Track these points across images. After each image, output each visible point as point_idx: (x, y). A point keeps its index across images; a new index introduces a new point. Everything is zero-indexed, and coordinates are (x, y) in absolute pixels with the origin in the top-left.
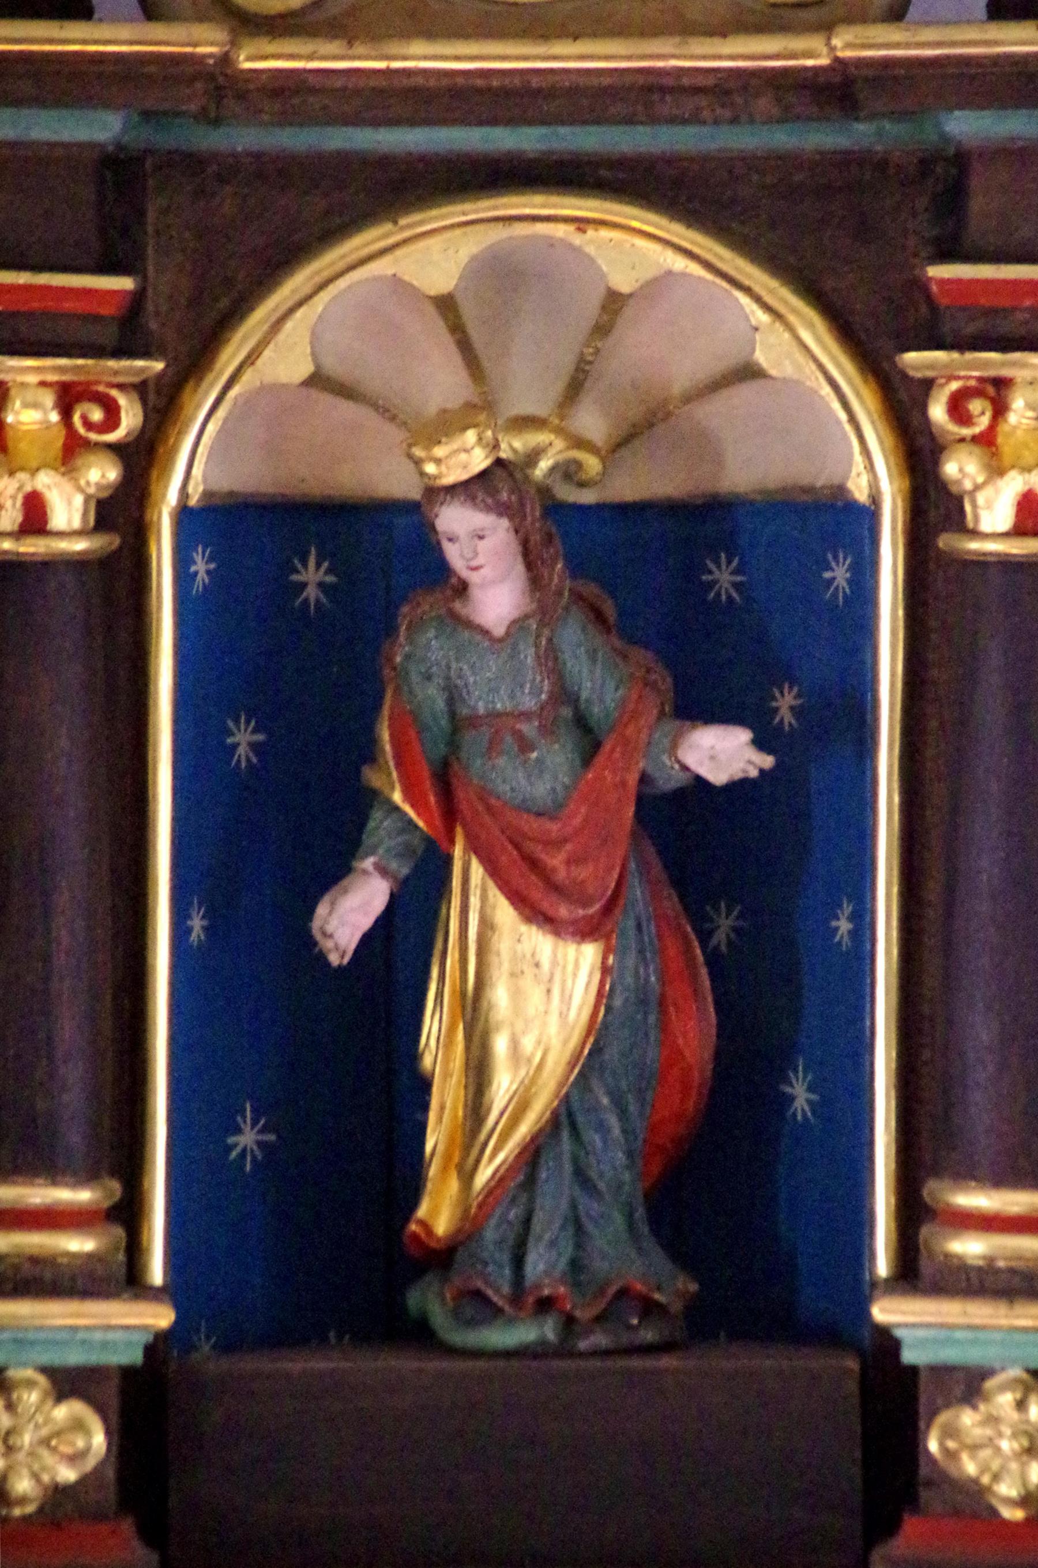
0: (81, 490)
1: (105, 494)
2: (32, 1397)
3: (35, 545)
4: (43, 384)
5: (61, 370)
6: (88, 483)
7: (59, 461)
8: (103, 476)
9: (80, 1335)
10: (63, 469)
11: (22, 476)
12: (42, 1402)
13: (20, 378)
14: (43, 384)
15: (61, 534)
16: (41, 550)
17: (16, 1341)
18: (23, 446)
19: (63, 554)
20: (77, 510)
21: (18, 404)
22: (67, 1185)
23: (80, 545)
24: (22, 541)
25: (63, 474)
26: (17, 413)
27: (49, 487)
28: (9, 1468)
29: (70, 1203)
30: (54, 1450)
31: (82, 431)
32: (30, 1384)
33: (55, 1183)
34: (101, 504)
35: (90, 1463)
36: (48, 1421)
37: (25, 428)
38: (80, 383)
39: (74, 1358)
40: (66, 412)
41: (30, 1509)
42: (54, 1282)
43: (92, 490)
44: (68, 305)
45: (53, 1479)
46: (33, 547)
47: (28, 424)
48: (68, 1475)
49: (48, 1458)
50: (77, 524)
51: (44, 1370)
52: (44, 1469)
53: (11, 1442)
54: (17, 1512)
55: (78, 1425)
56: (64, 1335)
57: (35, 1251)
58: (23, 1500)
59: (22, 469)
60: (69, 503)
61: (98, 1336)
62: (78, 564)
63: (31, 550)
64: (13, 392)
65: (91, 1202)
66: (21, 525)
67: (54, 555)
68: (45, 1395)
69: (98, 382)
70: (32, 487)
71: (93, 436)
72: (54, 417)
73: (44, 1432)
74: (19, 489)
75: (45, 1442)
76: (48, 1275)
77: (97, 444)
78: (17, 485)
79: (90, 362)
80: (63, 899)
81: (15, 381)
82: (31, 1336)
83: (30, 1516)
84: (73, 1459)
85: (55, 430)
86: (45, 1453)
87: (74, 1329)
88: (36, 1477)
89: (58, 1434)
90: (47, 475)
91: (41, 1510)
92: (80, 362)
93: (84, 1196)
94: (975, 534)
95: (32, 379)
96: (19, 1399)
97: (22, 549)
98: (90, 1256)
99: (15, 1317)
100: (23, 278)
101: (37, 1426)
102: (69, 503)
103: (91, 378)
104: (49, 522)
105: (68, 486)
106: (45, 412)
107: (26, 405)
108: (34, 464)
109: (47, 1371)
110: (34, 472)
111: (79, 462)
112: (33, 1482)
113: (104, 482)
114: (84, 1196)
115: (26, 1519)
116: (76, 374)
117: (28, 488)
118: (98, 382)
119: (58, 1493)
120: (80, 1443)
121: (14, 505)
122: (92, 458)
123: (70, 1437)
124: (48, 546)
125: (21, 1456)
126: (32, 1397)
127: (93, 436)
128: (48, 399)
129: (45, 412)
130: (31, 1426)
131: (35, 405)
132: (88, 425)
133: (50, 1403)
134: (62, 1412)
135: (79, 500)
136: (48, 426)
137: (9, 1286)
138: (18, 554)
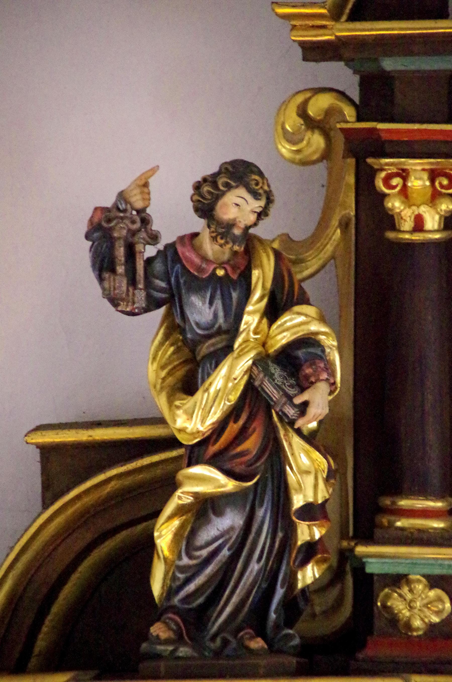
0: (438, 213)
1: (447, 215)
2: (420, 587)
3: (419, 236)
4: (424, 170)
5: (431, 164)
6: (441, 210)
7: (429, 201)
8: (448, 207)
9: (440, 562)
10: (430, 205)
11: (414, 208)
12: (424, 589)
13: (413, 168)
14: (424, 170)
15: (404, 232)
16: (421, 238)
17: (412, 563)
18: (415, 195)
19: (431, 239)
20: (436, 221)
21: (413, 178)
22: (432, 500)
23: (437, 236)
24: (413, 235)
25: (431, 207)
26: (412, 182)
27: (425, 212)
28: (412, 616)
29: (433, 507)
30: (429, 608)
31: (439, 189)
32: (419, 581)
33: (427, 499)
34: (446, 219)
35: (445, 615)
36: (427, 597)
37: (415, 188)
38: (439, 169)
39: (437, 571)
40: (432, 180)
41: (420, 633)
42: (428, 540)
43: (443, 213)
44: (435, 138)
45: (430, 621)
46: (418, 237)
47: (417, 186)
48: (435, 619)
49: (428, 613)
50: (436, 227)
51: (424, 576)
52: (426, 617)
53: (411, 605)
54: (415, 634)
55: (440, 600)
56: (433, 562)
57: (420, 527)
58: (418, 629)
59: (414, 205)
60: (433, 218)
61: (447, 562)
62: (436, 243)
63: (417, 238)
64: (411, 174)
65: (443, 507)
66: (413, 228)
67: (427, 240)
68: (425, 586)
69: (445, 169)
70: (418, 212)
71: (444, 191)
72: (428, 183)
73: (425, 601)
74: (413, 213)
75: (426, 606)
76: (425, 537)
77: (445, 194)
78: (411, 211)
79: (443, 160)
80: (429, 383)
81: (412, 169)
82: (418, 562)
83: (420, 635)
84: (437, 613)
85: (428, 189)
86: (426, 610)
87: (437, 559)
88: (422, 620)
89: (430, 603)
90: (424, 207)
91: (425, 634)
92: (439, 160)
93: (439, 504)
94: (400, 231)
95: (419, 168)
96: (415, 587)
97: (413, 238)
98: (442, 529)
99: (411, 553)
100: (416, 126)
101: (422, 599)
102: (433, 218)
103: (443, 167)
104: (425, 226)
105: (432, 211)
106: (424, 181)
107: (416, 179)
108: (419, 203)
109: (427, 577)
110: (418, 206)
111: (437, 202)
112: (421, 622)
113: (448, 209)
114: (439, 504)
115: (418, 637)
116: (437, 165)
117: (416, 213)
118: (445, 169)
119: (432, 627)
120: (440, 607)
121: (410, 220)
122: (443, 200)
123: (436, 604)
124: (424, 237)
125: (416, 611)
126: (420, 587)
127: (444, 191)
128: (425, 176)
129: (424, 181)
130: (420, 599)
131: (420, 179)
132: (442, 186)
133: (427, 590)
134: (432, 593)
135: (437, 217)
136: (425, 187)
137: (410, 541)
138: (412, 240)
